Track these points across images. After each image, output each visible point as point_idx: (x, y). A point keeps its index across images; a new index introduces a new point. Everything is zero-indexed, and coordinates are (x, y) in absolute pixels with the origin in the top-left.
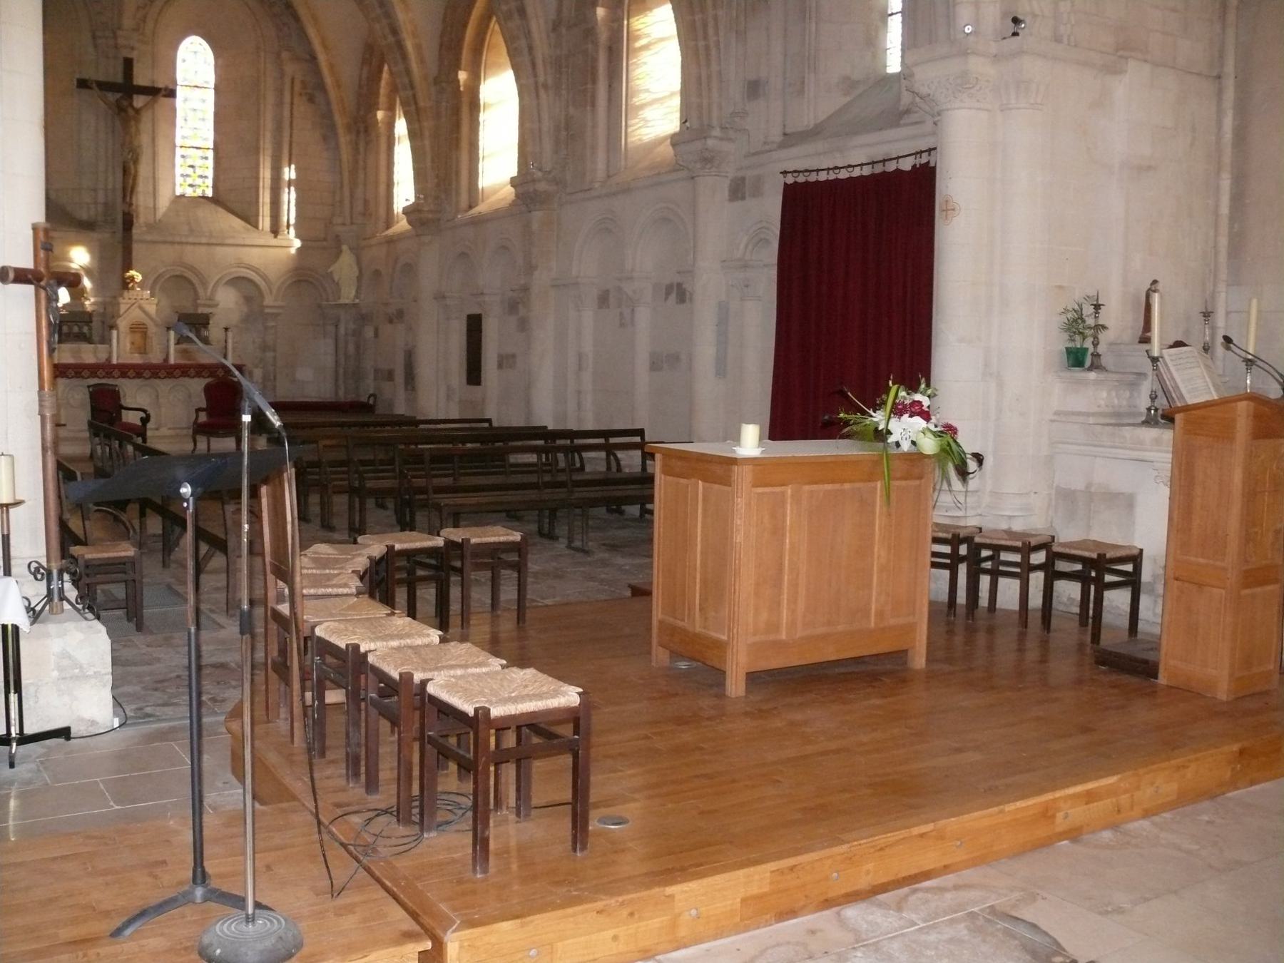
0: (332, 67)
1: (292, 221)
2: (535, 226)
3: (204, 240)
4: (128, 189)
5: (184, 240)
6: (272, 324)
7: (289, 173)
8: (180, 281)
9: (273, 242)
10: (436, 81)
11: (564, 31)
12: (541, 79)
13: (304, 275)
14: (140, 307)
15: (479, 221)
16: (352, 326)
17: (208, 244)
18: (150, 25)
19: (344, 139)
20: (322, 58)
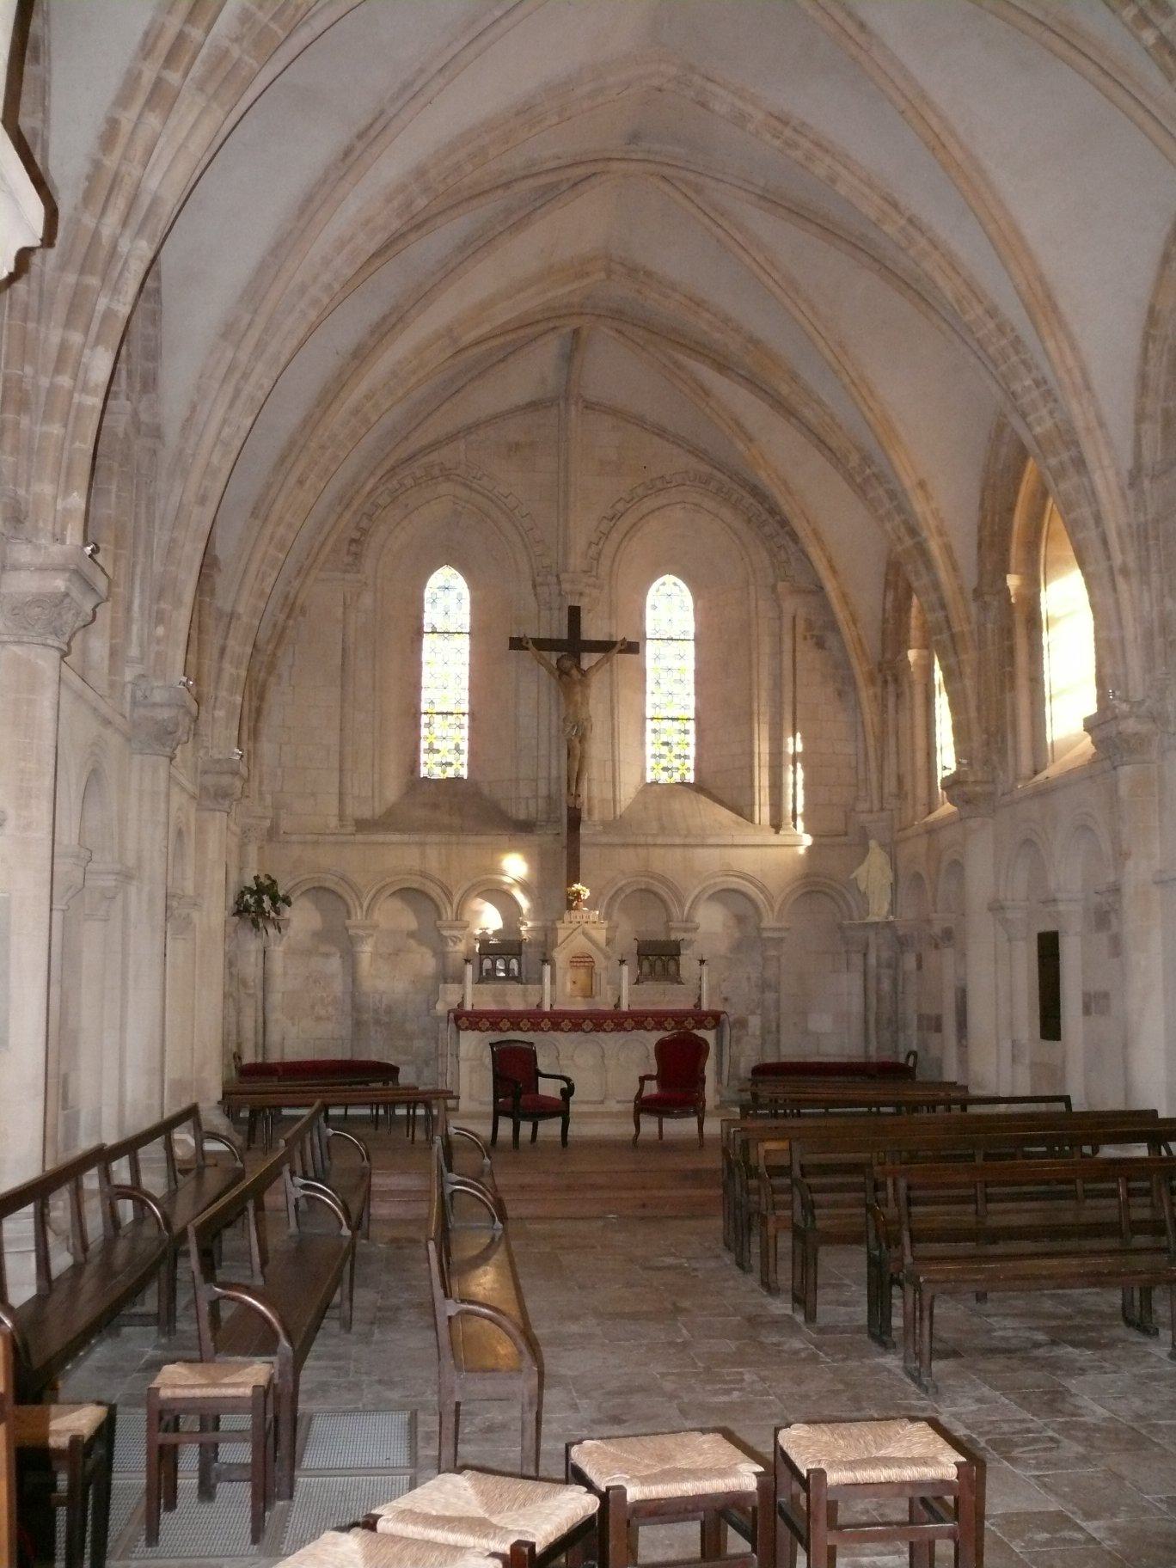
0: (844, 596)
1: (800, 810)
2: (1124, 790)
3: (678, 841)
4: (575, 778)
5: (650, 840)
6: (772, 953)
7: (794, 744)
8: (649, 894)
9: (774, 839)
10: (978, 593)
11: (1146, 484)
12: (1118, 559)
13: (817, 884)
14: (585, 934)
15: (1046, 792)
16: (885, 955)
17: (684, 846)
18: (605, 563)
19: (866, 693)
20: (830, 586)
